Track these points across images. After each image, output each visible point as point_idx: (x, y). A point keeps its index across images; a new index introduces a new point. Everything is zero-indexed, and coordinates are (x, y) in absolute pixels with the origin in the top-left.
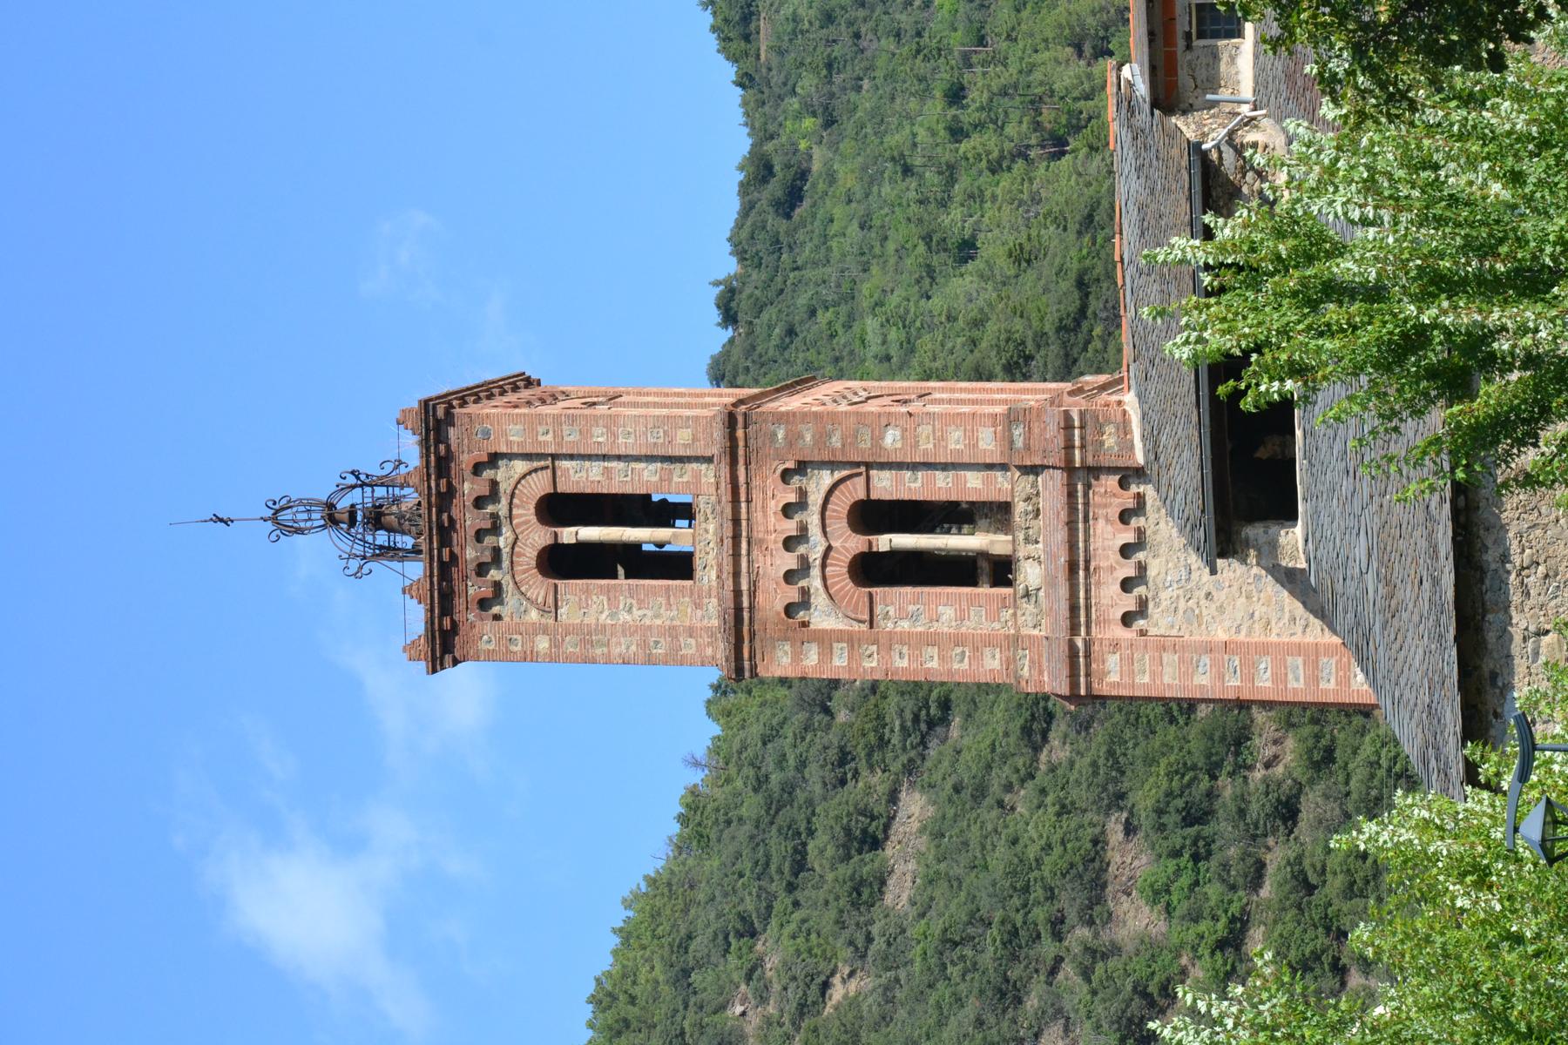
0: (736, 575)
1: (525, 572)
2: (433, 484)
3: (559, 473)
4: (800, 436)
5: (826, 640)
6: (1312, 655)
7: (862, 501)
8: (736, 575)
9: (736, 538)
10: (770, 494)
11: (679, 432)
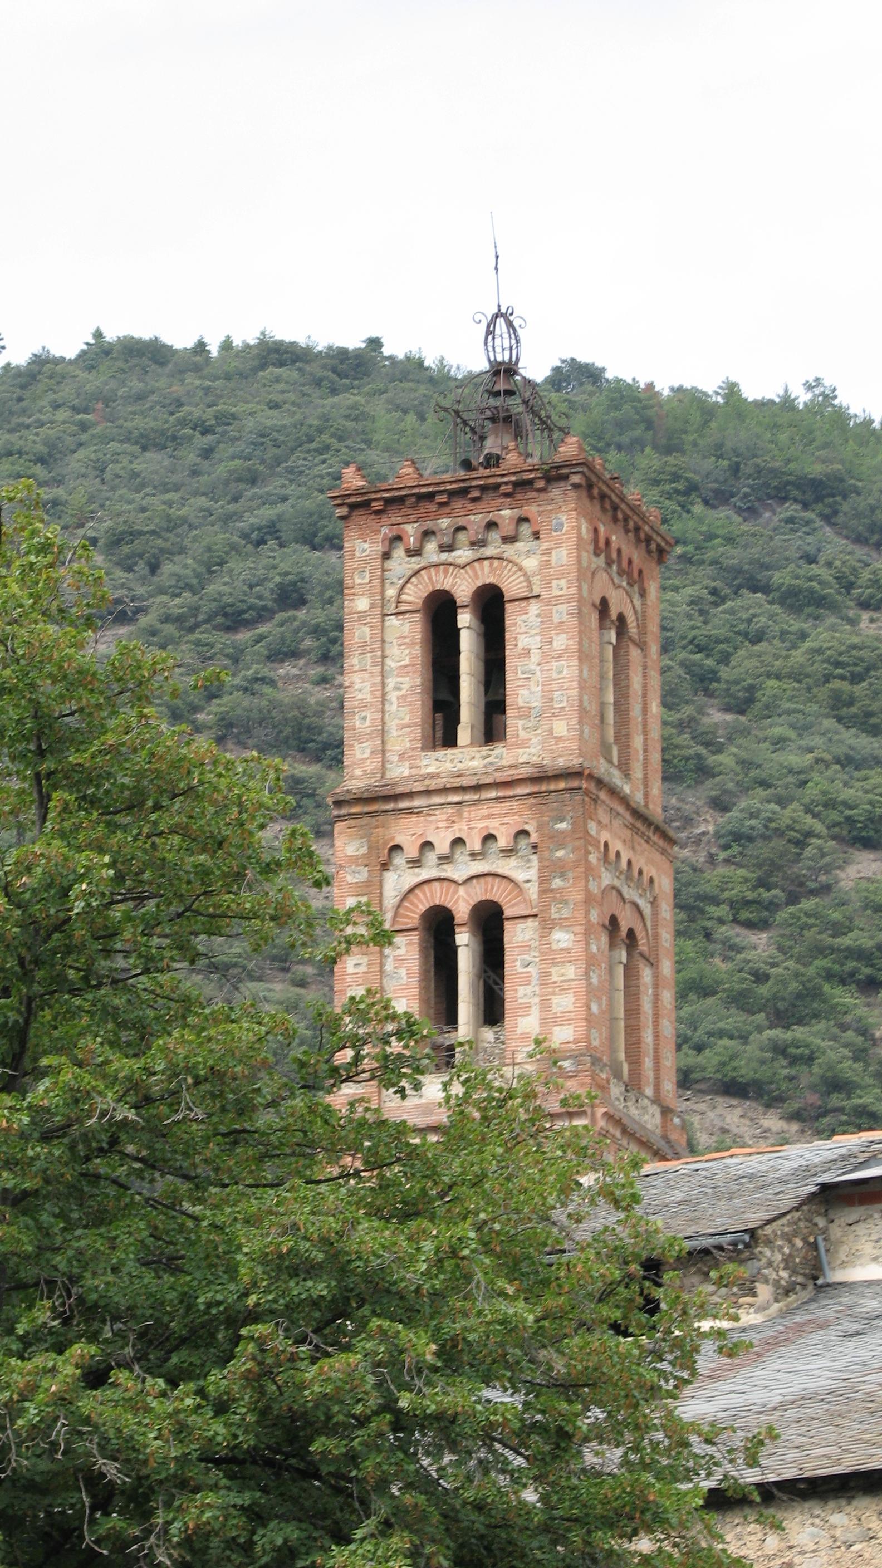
0: (428, 793)
1: (430, 578)
2: (505, 479)
3: (524, 604)
4: (561, 846)
7: (453, 918)
8: (428, 793)
9: (464, 789)
10: (506, 820)
11: (564, 723)
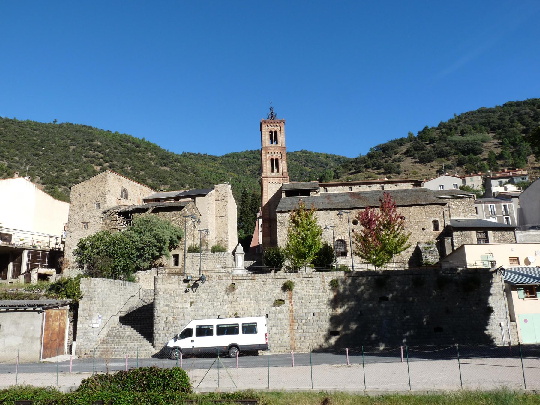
5: (266, 156)
6: (267, 199)
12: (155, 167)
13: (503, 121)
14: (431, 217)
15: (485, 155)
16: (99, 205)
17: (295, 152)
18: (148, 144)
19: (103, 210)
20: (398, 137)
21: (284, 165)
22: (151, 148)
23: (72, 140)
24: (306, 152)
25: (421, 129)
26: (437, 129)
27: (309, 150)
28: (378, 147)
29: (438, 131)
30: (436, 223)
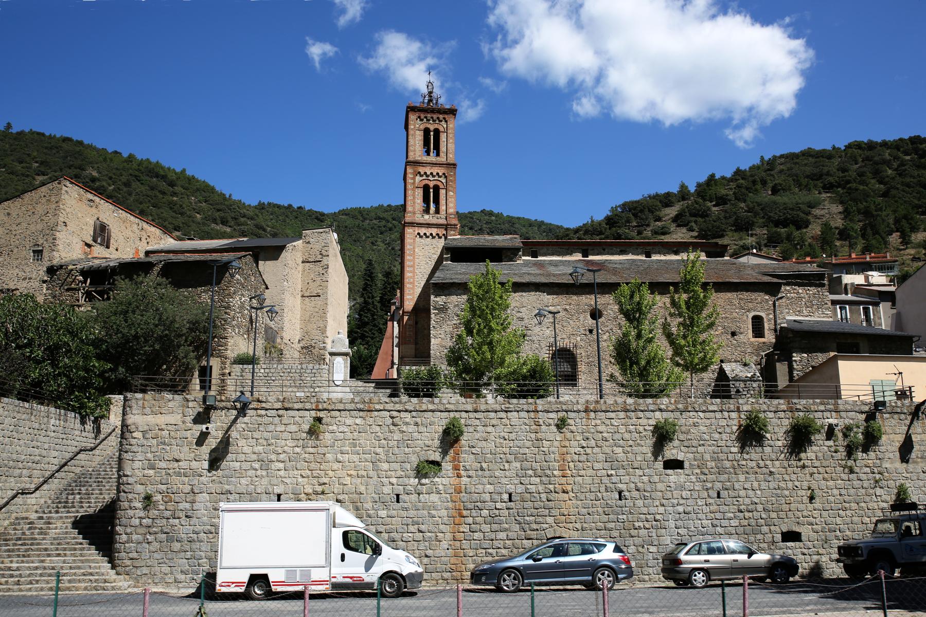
5: (414, 179)
12: (204, 224)
13: (846, 174)
14: (749, 311)
15: (815, 229)
16: (38, 253)
17: (470, 213)
18: (191, 180)
19: (47, 264)
20: (662, 191)
21: (449, 200)
22: (198, 190)
23: (42, 163)
24: (491, 214)
25: (703, 179)
26: (731, 180)
27: (496, 211)
28: (624, 205)
29: (733, 185)
30: (757, 322)
